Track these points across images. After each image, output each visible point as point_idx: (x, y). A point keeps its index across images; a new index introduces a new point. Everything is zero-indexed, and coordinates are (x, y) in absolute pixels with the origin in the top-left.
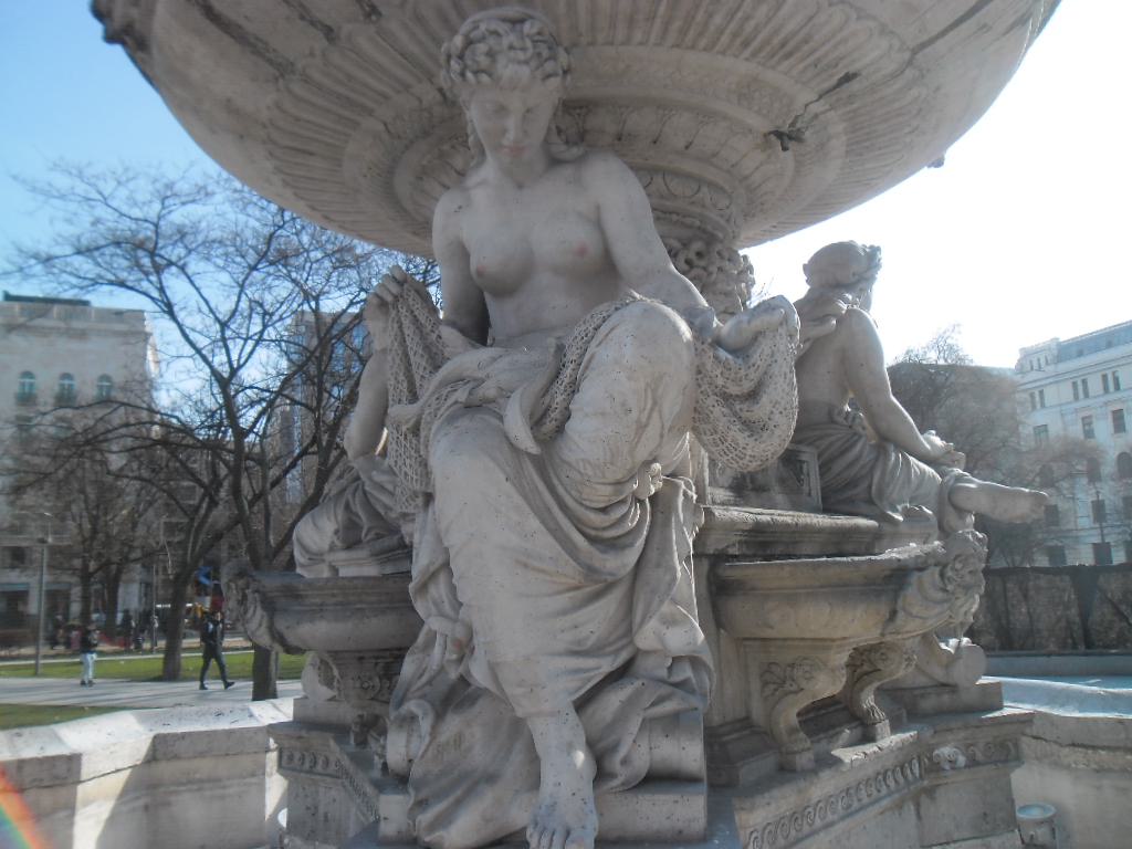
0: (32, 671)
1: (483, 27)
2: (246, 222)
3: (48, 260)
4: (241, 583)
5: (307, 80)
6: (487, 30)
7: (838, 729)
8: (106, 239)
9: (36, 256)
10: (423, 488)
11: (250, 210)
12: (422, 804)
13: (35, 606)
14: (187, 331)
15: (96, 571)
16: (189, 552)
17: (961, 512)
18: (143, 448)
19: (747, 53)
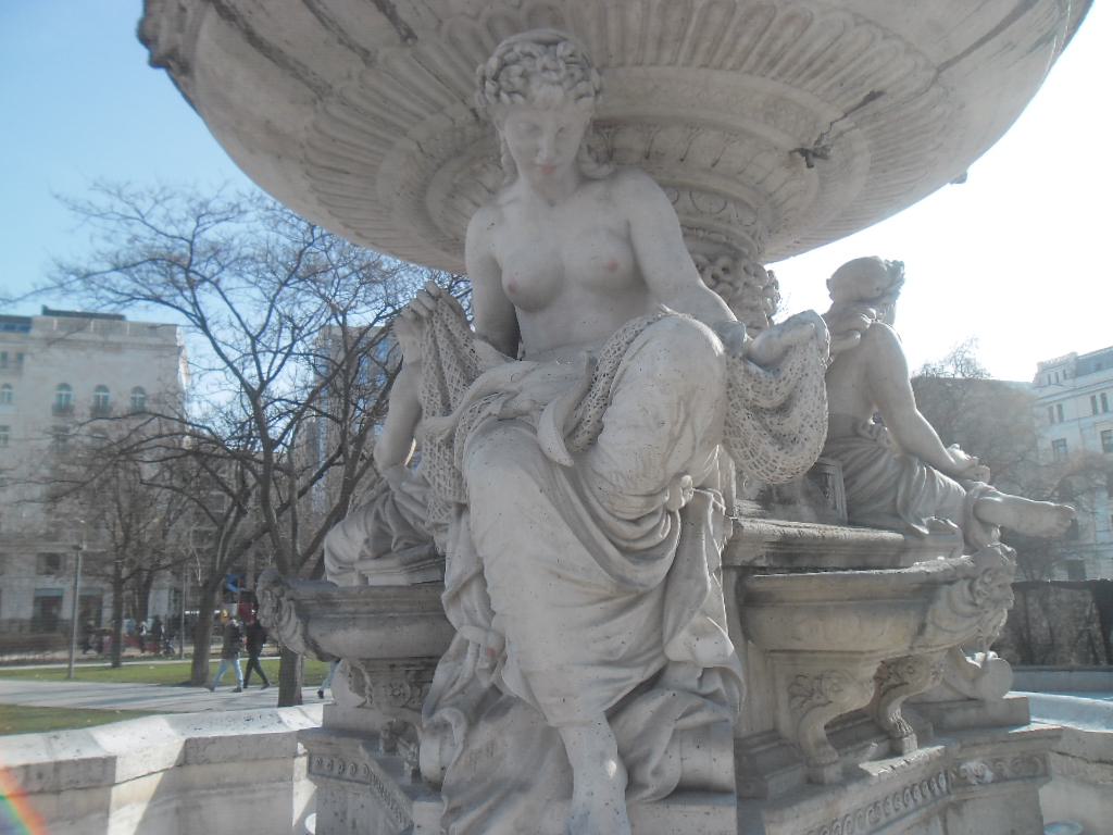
0: (66, 675)
1: (517, 49)
2: (277, 240)
3: (87, 276)
4: (276, 590)
5: (344, 102)
6: (521, 52)
7: (865, 743)
8: (143, 256)
9: (76, 272)
10: (457, 498)
11: (281, 227)
12: (455, 812)
13: (68, 611)
14: (220, 345)
15: (128, 578)
16: (218, 561)
17: (987, 526)
18: (174, 459)
19: (773, 73)
